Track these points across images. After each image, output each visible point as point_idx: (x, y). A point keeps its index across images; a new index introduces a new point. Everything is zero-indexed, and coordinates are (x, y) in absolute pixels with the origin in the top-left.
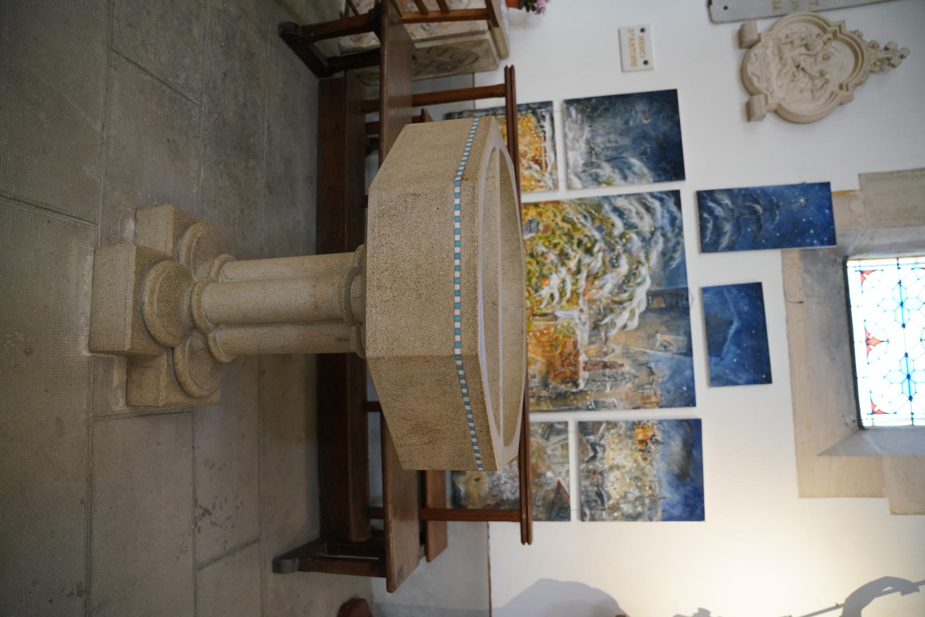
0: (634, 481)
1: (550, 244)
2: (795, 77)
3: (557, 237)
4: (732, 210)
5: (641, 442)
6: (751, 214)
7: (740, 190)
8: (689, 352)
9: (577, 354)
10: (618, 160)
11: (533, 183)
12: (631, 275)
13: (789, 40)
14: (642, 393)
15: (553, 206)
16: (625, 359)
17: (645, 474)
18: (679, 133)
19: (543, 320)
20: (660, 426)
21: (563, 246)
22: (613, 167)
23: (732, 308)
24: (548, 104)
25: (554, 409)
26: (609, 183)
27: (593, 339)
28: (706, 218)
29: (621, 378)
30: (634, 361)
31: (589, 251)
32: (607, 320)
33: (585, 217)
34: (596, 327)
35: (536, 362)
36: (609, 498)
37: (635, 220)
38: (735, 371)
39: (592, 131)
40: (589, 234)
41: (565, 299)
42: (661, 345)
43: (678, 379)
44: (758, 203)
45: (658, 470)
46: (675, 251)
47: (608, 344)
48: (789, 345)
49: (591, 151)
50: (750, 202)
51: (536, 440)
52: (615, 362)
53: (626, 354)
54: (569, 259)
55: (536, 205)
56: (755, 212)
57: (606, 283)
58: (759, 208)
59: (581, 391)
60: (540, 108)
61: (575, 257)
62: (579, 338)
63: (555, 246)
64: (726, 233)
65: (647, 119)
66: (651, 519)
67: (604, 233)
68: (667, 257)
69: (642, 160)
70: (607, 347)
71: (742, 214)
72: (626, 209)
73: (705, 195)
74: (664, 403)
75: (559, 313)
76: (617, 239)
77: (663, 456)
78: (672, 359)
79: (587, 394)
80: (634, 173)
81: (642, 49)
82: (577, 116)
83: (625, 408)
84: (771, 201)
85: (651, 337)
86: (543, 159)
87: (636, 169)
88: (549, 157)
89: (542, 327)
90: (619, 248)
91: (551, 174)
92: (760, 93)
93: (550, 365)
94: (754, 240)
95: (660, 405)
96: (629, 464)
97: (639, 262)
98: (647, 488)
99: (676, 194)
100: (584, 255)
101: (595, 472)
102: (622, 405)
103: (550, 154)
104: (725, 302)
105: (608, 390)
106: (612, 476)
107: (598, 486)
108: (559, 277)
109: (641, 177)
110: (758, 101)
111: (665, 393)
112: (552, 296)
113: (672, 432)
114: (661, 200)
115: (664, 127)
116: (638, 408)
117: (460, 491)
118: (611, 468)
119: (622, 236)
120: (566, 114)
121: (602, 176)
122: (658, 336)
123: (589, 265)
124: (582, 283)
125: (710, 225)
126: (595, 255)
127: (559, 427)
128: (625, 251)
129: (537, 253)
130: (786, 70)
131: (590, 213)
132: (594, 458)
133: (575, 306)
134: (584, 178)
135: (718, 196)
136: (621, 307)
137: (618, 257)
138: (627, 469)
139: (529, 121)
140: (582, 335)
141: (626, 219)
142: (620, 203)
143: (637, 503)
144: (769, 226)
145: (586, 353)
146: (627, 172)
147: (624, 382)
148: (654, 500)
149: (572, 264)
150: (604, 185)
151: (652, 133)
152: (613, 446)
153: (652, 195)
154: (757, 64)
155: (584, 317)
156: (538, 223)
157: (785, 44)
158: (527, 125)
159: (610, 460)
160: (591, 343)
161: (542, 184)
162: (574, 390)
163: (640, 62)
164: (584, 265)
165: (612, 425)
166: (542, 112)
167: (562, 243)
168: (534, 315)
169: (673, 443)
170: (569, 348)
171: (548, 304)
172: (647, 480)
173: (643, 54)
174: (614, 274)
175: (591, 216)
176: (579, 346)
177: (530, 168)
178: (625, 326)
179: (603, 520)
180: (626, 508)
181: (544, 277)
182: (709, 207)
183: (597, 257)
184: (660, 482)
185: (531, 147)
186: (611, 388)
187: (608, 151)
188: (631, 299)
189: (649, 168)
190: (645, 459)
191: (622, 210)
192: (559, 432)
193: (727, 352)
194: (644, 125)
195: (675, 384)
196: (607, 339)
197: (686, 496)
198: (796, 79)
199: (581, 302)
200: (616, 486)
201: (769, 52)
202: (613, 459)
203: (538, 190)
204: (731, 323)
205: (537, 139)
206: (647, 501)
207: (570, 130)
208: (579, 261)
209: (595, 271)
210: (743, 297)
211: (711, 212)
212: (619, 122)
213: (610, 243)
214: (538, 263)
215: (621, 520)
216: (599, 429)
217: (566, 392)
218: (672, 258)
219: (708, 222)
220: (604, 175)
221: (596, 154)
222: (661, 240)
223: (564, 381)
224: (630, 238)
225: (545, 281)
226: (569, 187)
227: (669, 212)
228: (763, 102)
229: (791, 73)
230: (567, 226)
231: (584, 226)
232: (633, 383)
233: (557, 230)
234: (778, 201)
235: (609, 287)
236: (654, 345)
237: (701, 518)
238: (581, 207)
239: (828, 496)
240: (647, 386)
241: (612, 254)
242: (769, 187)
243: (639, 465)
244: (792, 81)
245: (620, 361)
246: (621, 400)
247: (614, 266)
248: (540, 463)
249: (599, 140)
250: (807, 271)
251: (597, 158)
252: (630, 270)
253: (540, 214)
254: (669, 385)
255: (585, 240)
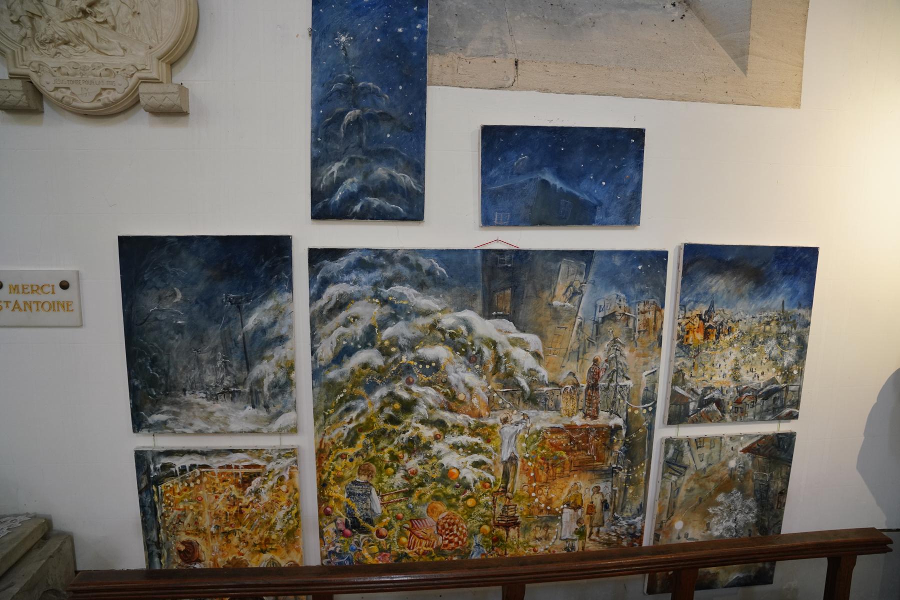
0: (757, 346)
1: (392, 466)
2: (106, 22)
3: (379, 454)
4: (352, 161)
5: (706, 336)
6: (360, 130)
7: (315, 144)
8: (586, 256)
9: (572, 428)
10: (248, 349)
11: (284, 488)
12: (453, 340)
13: (25, 20)
14: (639, 332)
15: (327, 459)
16: (587, 356)
17: (749, 332)
18: (202, 239)
19: (514, 477)
20: (688, 307)
21: (396, 446)
22: (261, 358)
23: (521, 180)
24: (141, 458)
25: (646, 460)
26: (290, 368)
27: (551, 404)
28: (362, 207)
29: (614, 362)
30: (591, 343)
31: (408, 407)
32: (524, 383)
33: (349, 410)
34: (533, 400)
35: (576, 487)
36: (773, 381)
37: (358, 329)
38: (619, 186)
39: (193, 389)
40: (378, 405)
41: (484, 445)
42: (570, 300)
43: (624, 276)
44: (343, 114)
45: (747, 312)
46: (419, 267)
47: (561, 382)
48: (584, 93)
49: (230, 394)
50: (339, 129)
51: (685, 482)
52: (590, 371)
53: (579, 354)
54: (419, 438)
55: (323, 485)
56: (357, 122)
57: (463, 381)
58: (350, 116)
59: (626, 422)
60: (148, 471)
61: (417, 428)
62: (548, 425)
63: (394, 458)
64: (391, 175)
65: (174, 295)
66: (808, 324)
67: (379, 381)
68: (428, 280)
69: (250, 310)
70: (565, 383)
71: (360, 146)
72: (338, 343)
73: (320, 205)
74: (657, 300)
75: (505, 456)
76: (390, 360)
77: (729, 304)
78: (594, 283)
79: (633, 412)
80: (274, 323)
81: (39, 289)
82: (163, 413)
83: (658, 360)
84: (339, 91)
85: (556, 315)
86: (241, 471)
87: (266, 320)
88: (239, 461)
89: (525, 479)
90: (406, 358)
91: (269, 460)
92: (135, 89)
93: (581, 467)
94: (409, 130)
95: (660, 307)
96: (734, 353)
97: (433, 326)
98: (768, 328)
99: (317, 256)
100: (415, 414)
101: (738, 402)
102: (653, 364)
103: (234, 459)
104: (510, 190)
105: (629, 383)
106: (747, 377)
107: (756, 397)
108: (447, 454)
109: (281, 313)
110: (149, 94)
111: (644, 298)
112: (476, 464)
113: (699, 289)
114: (326, 283)
115: (191, 264)
116: (660, 339)
117: (738, 578)
118: (736, 378)
119: (385, 352)
120: (160, 428)
121: (275, 377)
122: (556, 303)
123: (431, 407)
124: (460, 419)
125: (376, 202)
126: (414, 396)
127: (671, 451)
128: (413, 349)
129: (405, 486)
130: (88, 35)
131: (341, 401)
132: (719, 403)
133: (497, 430)
134: (279, 407)
135: (324, 183)
136: (504, 360)
137: (421, 361)
138: (740, 356)
139: (173, 489)
140: (543, 420)
141: (356, 343)
142: (326, 351)
143: (785, 342)
144: (384, 102)
145: (570, 415)
146: (271, 335)
147: (621, 360)
148: (785, 318)
149: (428, 433)
150: (293, 375)
151: (201, 287)
152: (707, 377)
153: (315, 297)
154: (76, 89)
155: (515, 418)
156: (355, 483)
157: (33, 28)
158: (179, 494)
159: (725, 380)
160: (557, 407)
161: (286, 475)
162: (624, 432)
163: (62, 295)
164: (430, 415)
165: (678, 377)
166: (155, 469)
167: (391, 448)
168: (505, 490)
169: (714, 289)
170: (561, 439)
171: (489, 470)
172: (757, 328)
173: (47, 289)
174: (450, 369)
175: (347, 401)
176: (561, 425)
177: (257, 492)
178: (536, 355)
179: (800, 389)
180: (789, 358)
181: (446, 476)
182: (343, 200)
183: (418, 394)
184: (763, 310)
185: (220, 489)
186: (628, 379)
187: (231, 366)
188: (493, 344)
189: (266, 297)
190: (730, 330)
191: (339, 349)
192: (679, 452)
193: (590, 195)
194: (184, 300)
195: (632, 283)
196: (553, 383)
197: (784, 274)
198: (110, 19)
199: (491, 422)
200: (759, 372)
201: (52, 63)
202: (724, 376)
203: (296, 480)
204: (545, 183)
205: (205, 479)
206: (784, 329)
207: (191, 425)
208: (423, 422)
209: (442, 398)
210: (505, 159)
211: (352, 198)
212: (177, 342)
213: (395, 372)
214: (421, 485)
215: (803, 364)
216: (683, 396)
217: (625, 444)
218: (430, 273)
219: (370, 204)
220: (275, 374)
221: (235, 386)
222: (397, 288)
223: (609, 447)
224: (389, 339)
225: (453, 474)
226: (293, 430)
227: (348, 270)
228: (154, 88)
229: (96, 27)
230: (362, 439)
231: (363, 412)
232: (623, 345)
233: (368, 455)
234: (341, 80)
235: (470, 378)
236: (570, 311)
237: (813, 252)
238: (330, 415)
239: (801, 66)
240: (631, 326)
241: (416, 370)
242: (314, 92)
243: (737, 339)
244: (114, 28)
245: (590, 364)
246: (645, 364)
247: (434, 367)
248: (716, 476)
249: (209, 378)
250: (462, 45)
251: (243, 384)
252: (445, 342)
253: (339, 479)
254: (632, 291)
255: (388, 411)
